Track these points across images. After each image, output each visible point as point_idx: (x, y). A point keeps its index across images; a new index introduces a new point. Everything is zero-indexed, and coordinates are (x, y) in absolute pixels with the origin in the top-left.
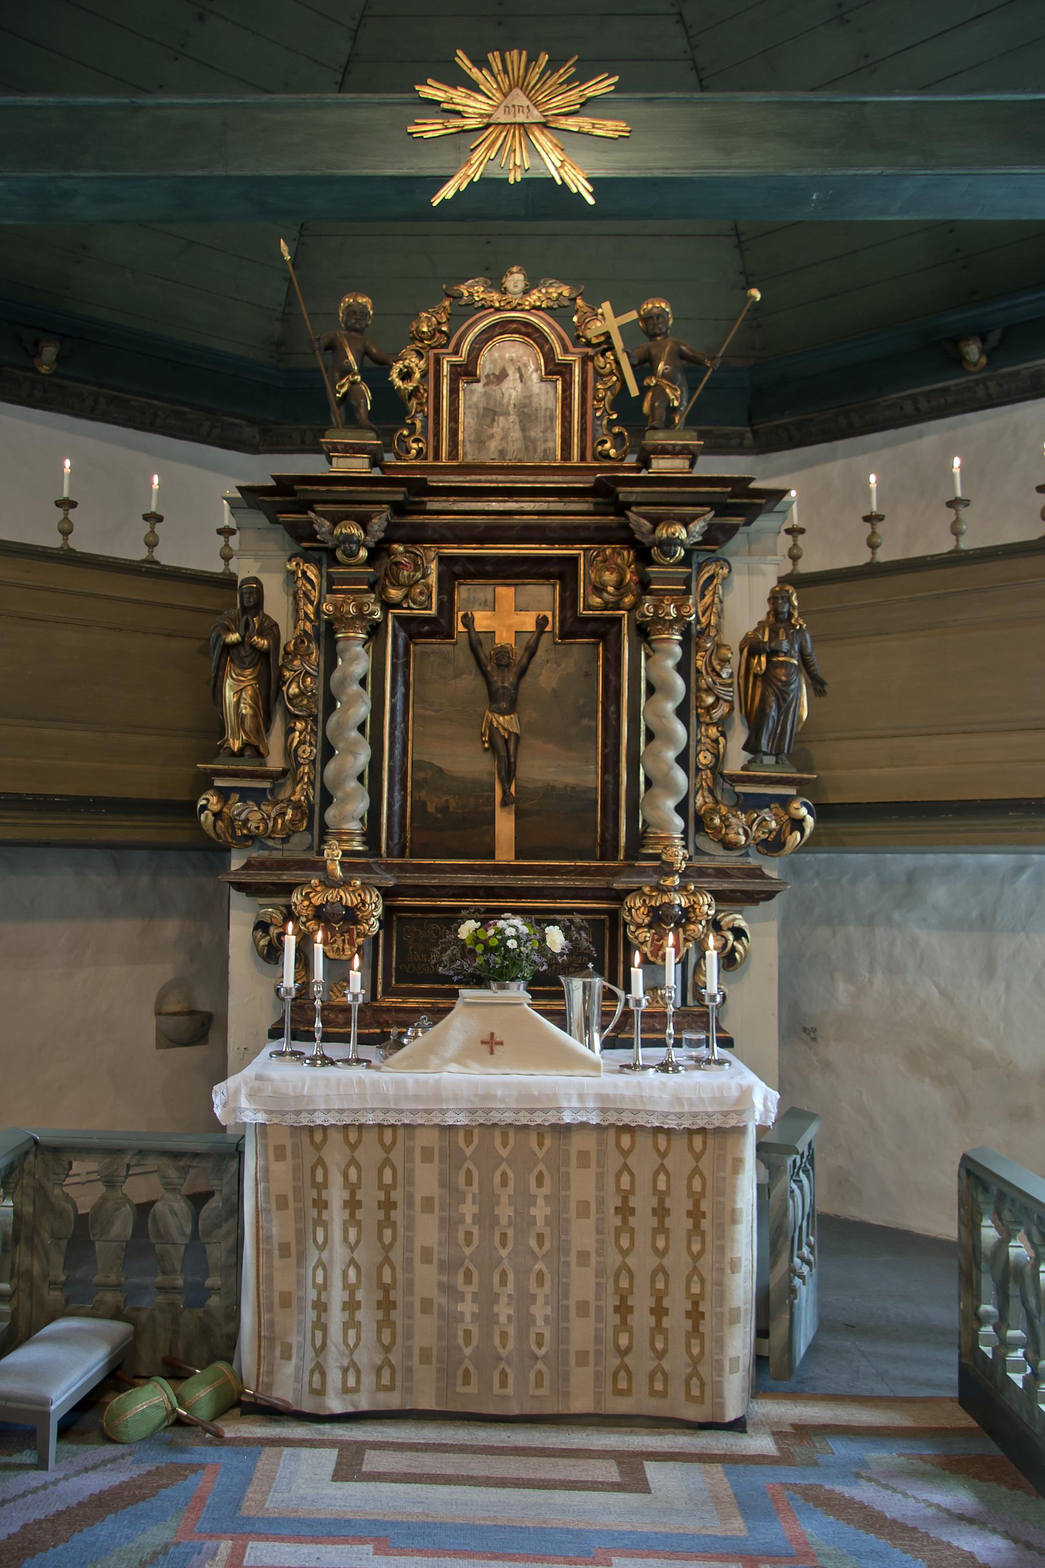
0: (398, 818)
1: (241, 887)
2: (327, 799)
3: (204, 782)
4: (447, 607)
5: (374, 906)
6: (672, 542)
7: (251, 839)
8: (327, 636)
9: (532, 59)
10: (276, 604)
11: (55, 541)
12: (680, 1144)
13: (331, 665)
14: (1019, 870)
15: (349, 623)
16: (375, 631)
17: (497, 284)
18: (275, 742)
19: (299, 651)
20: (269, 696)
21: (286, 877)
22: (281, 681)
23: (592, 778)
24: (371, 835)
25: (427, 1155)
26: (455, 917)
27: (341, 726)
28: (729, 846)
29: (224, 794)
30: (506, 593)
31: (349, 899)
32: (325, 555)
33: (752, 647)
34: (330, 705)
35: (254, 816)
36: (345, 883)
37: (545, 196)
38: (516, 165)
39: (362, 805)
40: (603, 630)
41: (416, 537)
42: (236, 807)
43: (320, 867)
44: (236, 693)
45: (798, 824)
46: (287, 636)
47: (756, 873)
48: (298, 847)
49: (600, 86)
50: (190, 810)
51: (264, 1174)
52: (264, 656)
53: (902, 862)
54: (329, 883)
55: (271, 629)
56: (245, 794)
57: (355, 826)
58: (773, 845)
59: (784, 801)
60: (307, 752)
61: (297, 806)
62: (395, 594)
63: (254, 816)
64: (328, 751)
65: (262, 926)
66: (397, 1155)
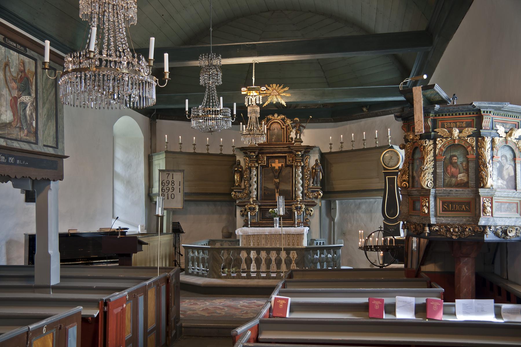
0: (261, 195)
1: (238, 206)
2: (250, 192)
3: (232, 190)
4: (268, 163)
5: (257, 207)
6: (298, 155)
7: (239, 199)
8: (250, 168)
9: (277, 85)
10: (242, 164)
11: (206, 152)
12: (296, 236)
13: (251, 173)
14: (375, 202)
15: (253, 167)
16: (257, 168)
17: (273, 116)
18: (243, 184)
19: (246, 171)
20: (241, 177)
21: (245, 204)
22: (243, 175)
23: (290, 189)
24: (257, 198)
25: (263, 238)
26: (269, 209)
27: (252, 182)
28: (310, 198)
29: (235, 192)
30: (277, 161)
31: (253, 206)
32: (250, 157)
33: (313, 168)
34: (251, 179)
35: (240, 195)
36: (253, 204)
37: (278, 105)
38: (275, 101)
39: (256, 193)
40: (291, 166)
41: (263, 153)
42: (237, 194)
43: (249, 202)
44: (237, 177)
45: (320, 194)
46: (244, 168)
47: (314, 202)
48: (246, 200)
49: (286, 89)
50: (230, 194)
51: (242, 241)
52: (241, 171)
53: (358, 201)
54: (251, 204)
55: (241, 167)
56: (238, 192)
57: (255, 196)
58: (316, 198)
59: (318, 191)
60: (247, 185)
61: (246, 194)
62: (260, 162)
63: (240, 195)
64: (250, 186)
65: (241, 211)
66: (259, 238)
